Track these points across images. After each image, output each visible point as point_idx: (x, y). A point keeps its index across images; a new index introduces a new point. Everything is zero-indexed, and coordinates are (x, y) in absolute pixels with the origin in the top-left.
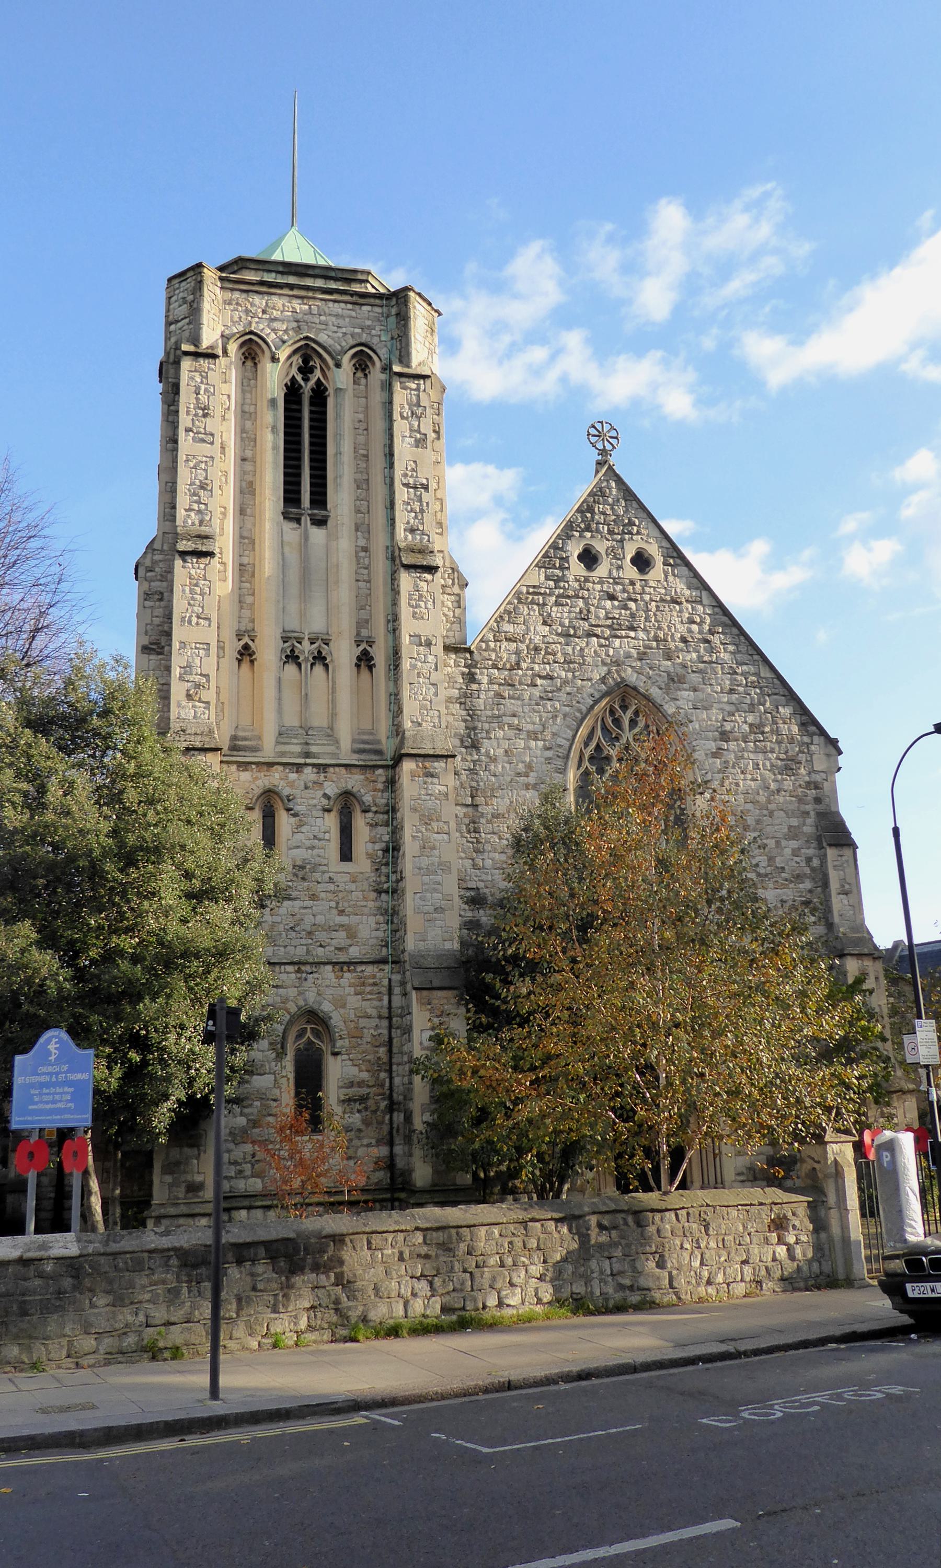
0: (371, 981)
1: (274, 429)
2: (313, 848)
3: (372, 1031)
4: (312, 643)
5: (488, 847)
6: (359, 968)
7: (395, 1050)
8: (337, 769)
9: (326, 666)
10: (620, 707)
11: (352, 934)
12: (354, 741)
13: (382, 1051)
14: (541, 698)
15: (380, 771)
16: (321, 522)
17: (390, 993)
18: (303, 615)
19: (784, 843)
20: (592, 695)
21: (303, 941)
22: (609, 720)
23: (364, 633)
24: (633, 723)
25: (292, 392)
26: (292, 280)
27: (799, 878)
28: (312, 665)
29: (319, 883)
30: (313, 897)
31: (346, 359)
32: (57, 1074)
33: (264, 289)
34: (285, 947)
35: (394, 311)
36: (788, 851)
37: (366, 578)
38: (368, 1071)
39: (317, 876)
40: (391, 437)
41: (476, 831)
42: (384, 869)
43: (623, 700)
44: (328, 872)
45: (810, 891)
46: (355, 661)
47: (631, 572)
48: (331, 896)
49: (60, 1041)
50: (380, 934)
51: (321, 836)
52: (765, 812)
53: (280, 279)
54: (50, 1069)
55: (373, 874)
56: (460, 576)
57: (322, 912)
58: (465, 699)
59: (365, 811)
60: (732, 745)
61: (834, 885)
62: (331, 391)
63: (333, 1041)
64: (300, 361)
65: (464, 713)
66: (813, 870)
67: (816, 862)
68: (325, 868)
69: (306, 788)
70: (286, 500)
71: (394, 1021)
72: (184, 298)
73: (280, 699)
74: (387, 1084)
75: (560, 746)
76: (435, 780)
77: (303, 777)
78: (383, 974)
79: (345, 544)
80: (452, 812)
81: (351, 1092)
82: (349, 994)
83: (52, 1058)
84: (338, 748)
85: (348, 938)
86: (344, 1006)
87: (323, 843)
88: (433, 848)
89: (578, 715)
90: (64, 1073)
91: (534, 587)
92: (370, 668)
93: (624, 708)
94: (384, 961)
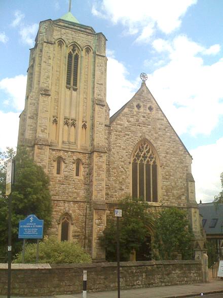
5: (112, 175)
11: (78, 194)
16: (75, 90)
18: (70, 113)
22: (141, 146)
25: (70, 55)
26: (72, 27)
27: (181, 188)
30: (69, 185)
39: (70, 179)
40: (94, 71)
41: (109, 171)
47: (148, 111)
49: (34, 217)
56: (109, 108)
57: (71, 189)
59: (83, 164)
60: (168, 155)
63: (72, 220)
67: (186, 185)
70: (67, 83)
71: (88, 218)
78: (85, 205)
79: (82, 96)
80: (104, 166)
81: (77, 234)
93: (144, 144)
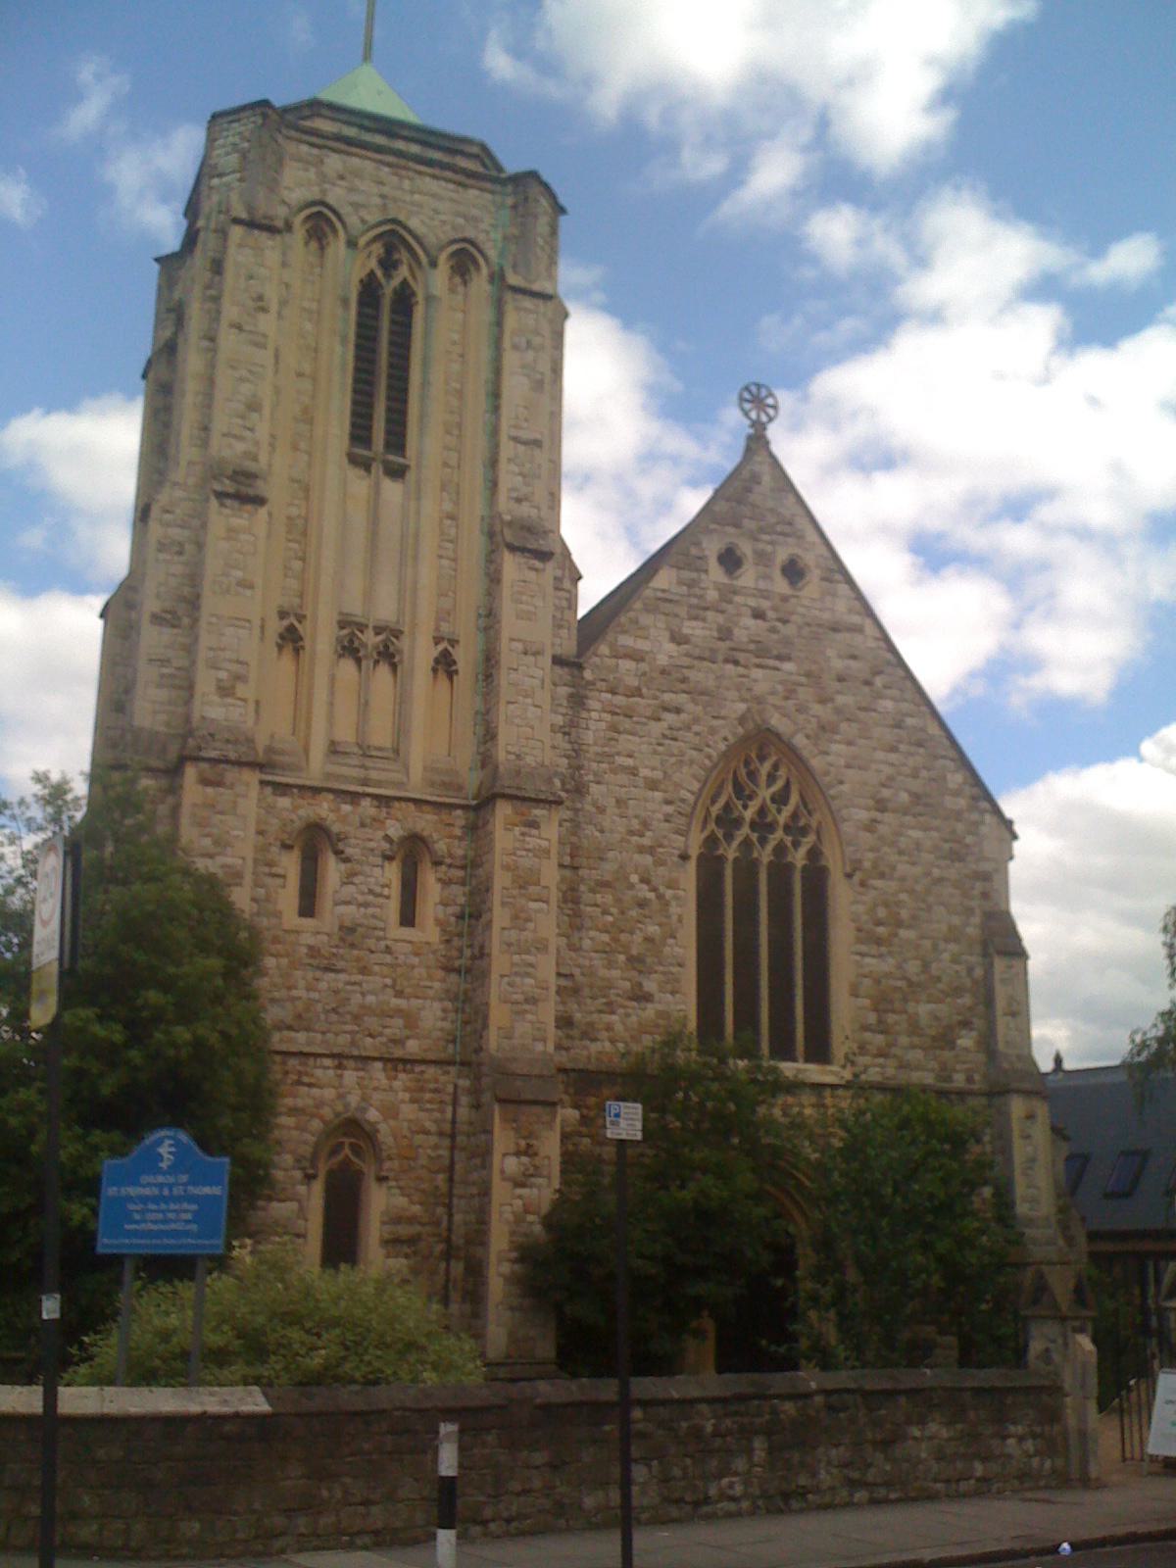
0: (432, 1086)
1: (344, 340)
2: (366, 905)
3: (429, 1151)
4: (377, 634)
5: (588, 923)
6: (418, 1069)
7: (457, 1178)
8: (403, 804)
9: (394, 667)
10: (758, 757)
11: (411, 1020)
12: (425, 768)
13: (441, 1179)
14: (664, 736)
15: (459, 812)
16: (397, 473)
17: (455, 1103)
19: (942, 945)
20: (725, 739)
21: (348, 1027)
22: (743, 772)
23: (445, 628)
24: (772, 778)
25: (369, 291)
27: (957, 991)
28: (377, 662)
29: (372, 952)
30: (364, 970)
31: (443, 257)
32: (170, 1187)
33: (343, 147)
34: (323, 1033)
35: (510, 201)
36: (946, 956)
37: (450, 554)
38: (421, 1204)
39: (371, 943)
42: (456, 942)
43: (761, 748)
44: (385, 939)
45: (970, 1009)
46: (432, 663)
47: (781, 586)
48: (385, 970)
49: (177, 1143)
50: (447, 1025)
51: (378, 890)
52: (923, 906)
53: (367, 137)
54: (161, 1179)
55: (442, 946)
58: (570, 729)
59: (437, 863)
60: (887, 817)
61: (1000, 1004)
62: (420, 297)
63: (379, 1161)
64: (382, 251)
65: (568, 746)
66: (975, 982)
67: (979, 972)
68: (381, 933)
69: (363, 825)
72: (234, 145)
73: (331, 704)
74: (445, 1224)
75: (683, 801)
76: (534, 832)
77: (360, 810)
78: (447, 1079)
79: (431, 507)
80: (551, 875)
82: (403, 1101)
83: (164, 1165)
84: (408, 774)
85: (405, 1027)
86: (395, 1116)
87: (381, 900)
88: (528, 920)
89: (707, 762)
90: (182, 1184)
91: (663, 591)
92: (451, 675)
93: (762, 758)
94: (450, 1063)
